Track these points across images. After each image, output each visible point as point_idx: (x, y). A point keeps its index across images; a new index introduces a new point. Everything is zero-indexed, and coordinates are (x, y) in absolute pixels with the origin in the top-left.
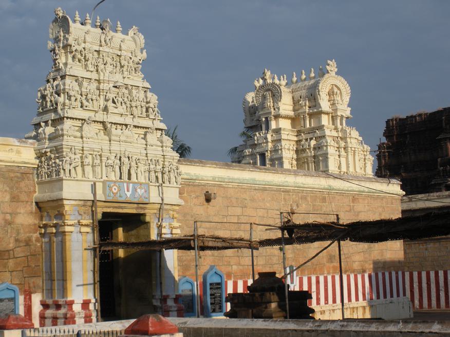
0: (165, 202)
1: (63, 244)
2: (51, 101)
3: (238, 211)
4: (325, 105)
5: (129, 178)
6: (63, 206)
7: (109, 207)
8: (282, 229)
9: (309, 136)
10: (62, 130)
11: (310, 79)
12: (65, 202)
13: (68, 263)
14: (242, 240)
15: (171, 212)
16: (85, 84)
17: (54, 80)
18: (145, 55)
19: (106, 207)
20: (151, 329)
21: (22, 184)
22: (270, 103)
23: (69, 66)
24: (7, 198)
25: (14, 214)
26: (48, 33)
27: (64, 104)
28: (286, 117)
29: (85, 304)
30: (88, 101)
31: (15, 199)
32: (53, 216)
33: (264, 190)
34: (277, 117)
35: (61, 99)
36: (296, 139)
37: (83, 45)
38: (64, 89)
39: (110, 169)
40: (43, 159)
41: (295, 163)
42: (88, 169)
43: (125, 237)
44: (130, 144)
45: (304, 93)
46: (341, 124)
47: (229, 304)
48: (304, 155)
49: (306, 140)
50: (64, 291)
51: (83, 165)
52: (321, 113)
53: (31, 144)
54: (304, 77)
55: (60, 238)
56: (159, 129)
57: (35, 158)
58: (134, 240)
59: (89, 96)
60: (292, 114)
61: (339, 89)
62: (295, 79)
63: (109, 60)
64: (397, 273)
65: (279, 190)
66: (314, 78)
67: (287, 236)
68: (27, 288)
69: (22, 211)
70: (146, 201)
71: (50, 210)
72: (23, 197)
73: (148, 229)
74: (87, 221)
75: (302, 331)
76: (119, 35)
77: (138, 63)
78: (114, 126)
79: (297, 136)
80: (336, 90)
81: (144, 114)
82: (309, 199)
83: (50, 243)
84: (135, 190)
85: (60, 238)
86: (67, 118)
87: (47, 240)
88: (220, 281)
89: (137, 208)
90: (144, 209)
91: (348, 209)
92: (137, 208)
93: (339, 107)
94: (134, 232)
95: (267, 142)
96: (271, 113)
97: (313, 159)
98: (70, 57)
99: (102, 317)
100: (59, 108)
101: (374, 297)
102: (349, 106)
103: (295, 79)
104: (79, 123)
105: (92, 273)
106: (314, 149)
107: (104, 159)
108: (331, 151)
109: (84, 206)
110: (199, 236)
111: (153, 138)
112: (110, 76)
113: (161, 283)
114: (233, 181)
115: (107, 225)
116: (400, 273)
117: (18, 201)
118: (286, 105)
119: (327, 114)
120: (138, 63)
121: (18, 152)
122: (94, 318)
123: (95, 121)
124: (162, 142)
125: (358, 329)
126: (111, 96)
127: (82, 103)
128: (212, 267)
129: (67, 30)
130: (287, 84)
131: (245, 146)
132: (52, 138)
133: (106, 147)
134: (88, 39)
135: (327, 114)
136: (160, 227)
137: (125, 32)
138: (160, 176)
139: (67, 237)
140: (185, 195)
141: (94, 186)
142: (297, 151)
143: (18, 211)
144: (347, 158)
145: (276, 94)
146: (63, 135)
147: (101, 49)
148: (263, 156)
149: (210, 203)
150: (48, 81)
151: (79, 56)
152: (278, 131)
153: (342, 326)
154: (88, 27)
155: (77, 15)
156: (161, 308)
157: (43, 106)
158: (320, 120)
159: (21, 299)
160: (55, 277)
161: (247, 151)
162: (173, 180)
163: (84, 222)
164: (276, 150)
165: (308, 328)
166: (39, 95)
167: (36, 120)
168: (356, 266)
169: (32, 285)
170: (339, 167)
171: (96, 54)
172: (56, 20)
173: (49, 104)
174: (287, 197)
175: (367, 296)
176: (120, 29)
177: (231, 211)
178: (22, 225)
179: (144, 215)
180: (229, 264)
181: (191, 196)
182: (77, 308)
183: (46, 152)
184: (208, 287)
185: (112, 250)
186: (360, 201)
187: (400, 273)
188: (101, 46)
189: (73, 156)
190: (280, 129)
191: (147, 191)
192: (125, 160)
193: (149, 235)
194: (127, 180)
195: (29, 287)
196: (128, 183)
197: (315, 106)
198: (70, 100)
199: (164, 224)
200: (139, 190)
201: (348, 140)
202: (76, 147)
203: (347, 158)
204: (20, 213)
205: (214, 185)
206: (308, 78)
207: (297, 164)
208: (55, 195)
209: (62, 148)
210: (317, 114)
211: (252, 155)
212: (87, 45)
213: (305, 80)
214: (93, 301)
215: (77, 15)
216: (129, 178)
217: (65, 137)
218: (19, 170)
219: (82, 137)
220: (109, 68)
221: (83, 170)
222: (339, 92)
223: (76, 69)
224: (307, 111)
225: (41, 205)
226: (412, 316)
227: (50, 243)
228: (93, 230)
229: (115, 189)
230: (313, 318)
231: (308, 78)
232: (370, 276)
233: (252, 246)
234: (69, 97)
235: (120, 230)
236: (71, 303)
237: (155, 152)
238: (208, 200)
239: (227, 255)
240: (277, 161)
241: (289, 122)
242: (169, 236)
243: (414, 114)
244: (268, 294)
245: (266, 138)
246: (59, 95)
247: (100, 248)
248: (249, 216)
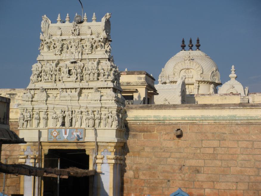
7: (55, 146)
19: (51, 145)
92: (77, 146)
114: (206, 119)
140: (155, 132)
141: (40, 133)
143: (15, 149)
177: (205, 143)
180: (201, 188)
181: (162, 133)
185: (3, 179)
191: (59, 133)
202: (28, 108)
204: (16, 150)
205: (184, 124)
218: (16, 124)
229: (55, 134)
239: (200, 180)
248: (228, 148)
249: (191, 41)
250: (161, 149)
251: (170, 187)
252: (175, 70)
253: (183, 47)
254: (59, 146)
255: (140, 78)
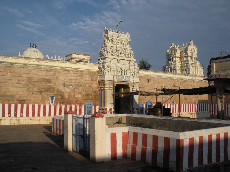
0: (134, 82)
1: (105, 92)
2: (103, 53)
3: (158, 85)
4: (189, 54)
5: (124, 75)
6: (105, 82)
8: (162, 90)
9: (184, 63)
10: (105, 61)
11: (186, 46)
12: (105, 81)
13: (106, 98)
14: (153, 93)
15: (136, 85)
16: (112, 48)
17: (104, 47)
18: (130, 40)
20: (96, 116)
21: (94, 76)
22: (173, 53)
23: (108, 43)
24: (90, 79)
25: (92, 84)
26: (103, 34)
27: (106, 54)
28: (178, 57)
29: (110, 109)
30: (113, 53)
31: (92, 80)
32: (102, 85)
33: (166, 79)
34: (175, 57)
35: (105, 53)
36: (181, 64)
37: (112, 37)
38: (106, 50)
39: (119, 72)
40: (100, 69)
41: (180, 71)
42: (112, 72)
43: (124, 91)
44: (125, 65)
45: (183, 50)
46: (194, 60)
47: (148, 111)
48: (183, 68)
49: (184, 64)
50: (105, 105)
51: (111, 71)
52: (188, 56)
53: (97, 65)
54: (184, 45)
55: (104, 91)
56: (134, 61)
57: (98, 69)
58: (126, 92)
59: (113, 52)
60: (180, 56)
61: (194, 49)
62: (181, 46)
63: (120, 42)
64: (206, 104)
65: (170, 79)
66: (187, 46)
67: (163, 92)
68: (95, 104)
69: (94, 83)
70: (129, 81)
71: (101, 83)
72: (95, 79)
73: (130, 89)
74: (112, 86)
75: (162, 119)
76: (123, 34)
77: (128, 42)
78: (120, 60)
79: (181, 63)
80: (193, 49)
81: (130, 57)
82: (179, 82)
83: (101, 92)
84: (126, 78)
85: (104, 91)
86: (107, 58)
87: (100, 91)
88: (151, 104)
89: (126, 83)
90: (128, 83)
91: (191, 85)
92: (126, 83)
93: (194, 54)
94: (126, 90)
95: (172, 64)
96: (173, 56)
97: (185, 70)
98: (108, 40)
99: (115, 113)
100: (105, 55)
101: (198, 110)
102: (197, 54)
103: (181, 46)
104: (110, 59)
105: (113, 101)
106: (186, 67)
107: (117, 69)
108: (191, 67)
109: (111, 82)
110: (140, 92)
111: (131, 63)
112: (120, 46)
113: (133, 104)
115: (118, 88)
116: (207, 104)
117: (93, 80)
118: (178, 54)
119: (190, 56)
120: (128, 42)
121: (93, 67)
122: (113, 113)
123: (115, 59)
124: (134, 65)
125: (176, 119)
126: (120, 52)
127: (111, 54)
128: (149, 100)
129: (108, 34)
130: (179, 48)
131: (166, 65)
132: (103, 63)
133: (118, 66)
134: (114, 36)
135: (190, 56)
136: (133, 89)
137: (125, 34)
138: (133, 74)
139: (106, 91)
142: (181, 67)
143: (93, 83)
144: (195, 70)
145: (175, 50)
146: (105, 63)
147: (117, 38)
148: (171, 68)
149: (149, 82)
150: (102, 48)
151: (111, 41)
152: (175, 61)
153: (172, 118)
154: (114, 32)
155: (111, 29)
156: (132, 111)
157: (101, 54)
158: (188, 58)
159: (93, 107)
160: (103, 102)
161: (167, 67)
162: (137, 75)
163: (111, 87)
164: (174, 67)
165: (163, 118)
166: (100, 51)
167: (99, 58)
168: (193, 102)
169: (96, 103)
170: (193, 72)
171: (116, 40)
172: (105, 31)
173: (102, 54)
174: (173, 81)
175: (196, 110)
176: (123, 33)
178: (94, 87)
179: (128, 85)
182: (108, 110)
183: (101, 67)
184: (147, 106)
186: (195, 82)
187: (207, 104)
188: (117, 37)
189: (108, 68)
190: (176, 61)
191: (129, 78)
192: (123, 70)
193: (130, 91)
194: (123, 75)
195: (96, 104)
196: (124, 76)
197: (186, 54)
198: (108, 53)
199: (134, 88)
200: (127, 78)
201: (196, 64)
203: (195, 70)
205: (151, 77)
206: (185, 46)
207: (181, 71)
208: (103, 79)
209: (105, 66)
210: (187, 56)
211: (168, 68)
212: (113, 38)
213: (184, 46)
214: (113, 108)
215: (111, 29)
216: (124, 75)
217: (106, 63)
219: (111, 63)
220: (120, 44)
221: (111, 72)
222: (194, 50)
223: (110, 44)
224: (184, 56)
225: (99, 82)
226: (210, 117)
227: (101, 92)
228: (113, 89)
230: (171, 116)
231: (185, 46)
232: (197, 105)
233: (157, 95)
234: (108, 52)
235: (122, 89)
236: (106, 109)
237: (132, 67)
238: (148, 81)
240: (175, 70)
241: (179, 58)
242: (135, 91)
243: (219, 57)
244: (158, 109)
245: (172, 63)
246: (105, 51)
247: (115, 94)
249: (33, 45)
250: (143, 86)
251: (146, 100)
252: (31, 55)
253: (30, 46)
254: (119, 83)
255: (88, 57)
